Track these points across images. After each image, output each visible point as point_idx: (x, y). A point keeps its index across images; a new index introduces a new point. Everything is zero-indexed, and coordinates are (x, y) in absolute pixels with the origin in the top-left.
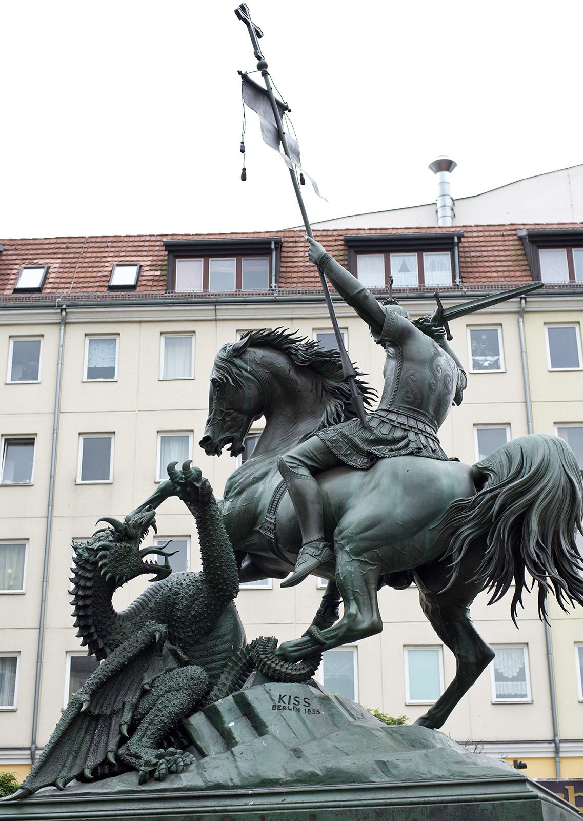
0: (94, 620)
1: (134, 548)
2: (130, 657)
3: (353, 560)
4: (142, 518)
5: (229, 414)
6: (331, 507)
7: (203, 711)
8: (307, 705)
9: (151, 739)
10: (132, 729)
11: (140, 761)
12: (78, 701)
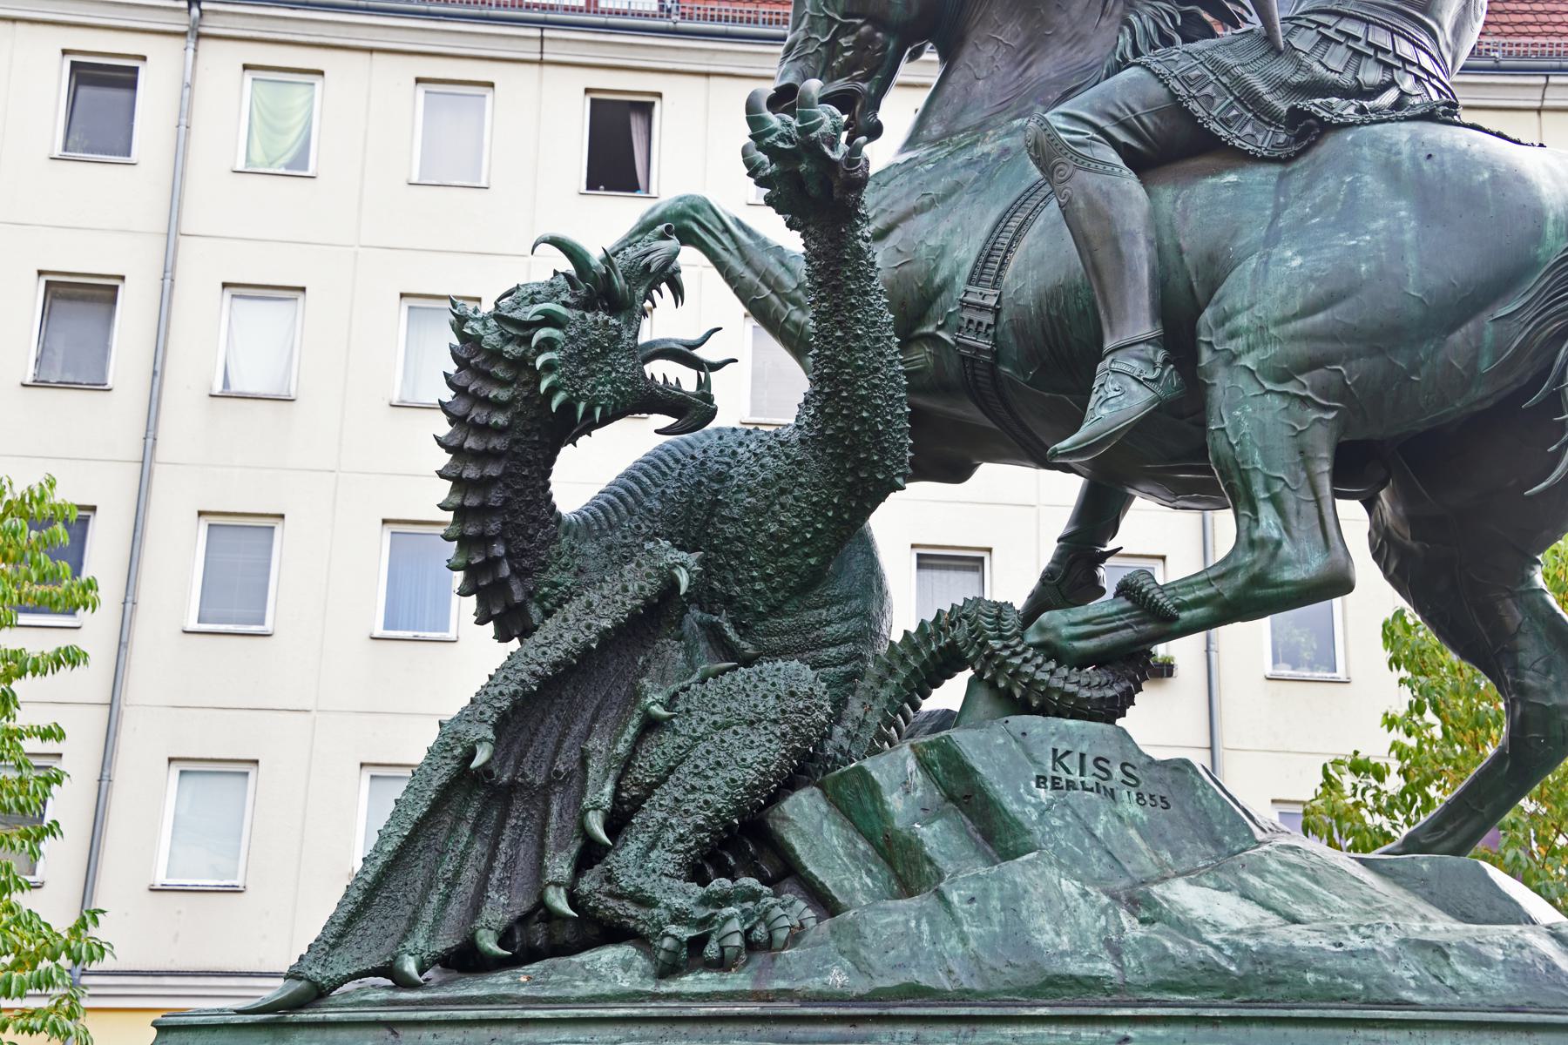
0: (504, 524)
1: (626, 334)
2: (607, 630)
3: (1268, 392)
4: (647, 255)
5: (845, 30)
6: (1186, 259)
7: (820, 786)
8: (1132, 782)
9: (676, 852)
10: (618, 822)
11: (656, 911)
12: (459, 739)
